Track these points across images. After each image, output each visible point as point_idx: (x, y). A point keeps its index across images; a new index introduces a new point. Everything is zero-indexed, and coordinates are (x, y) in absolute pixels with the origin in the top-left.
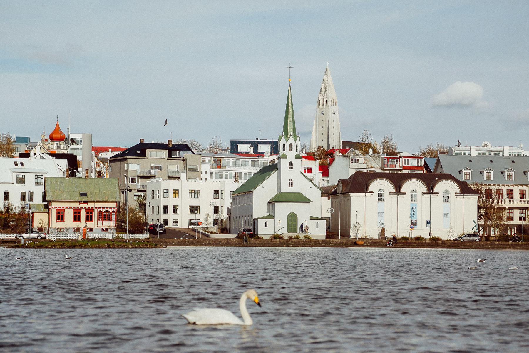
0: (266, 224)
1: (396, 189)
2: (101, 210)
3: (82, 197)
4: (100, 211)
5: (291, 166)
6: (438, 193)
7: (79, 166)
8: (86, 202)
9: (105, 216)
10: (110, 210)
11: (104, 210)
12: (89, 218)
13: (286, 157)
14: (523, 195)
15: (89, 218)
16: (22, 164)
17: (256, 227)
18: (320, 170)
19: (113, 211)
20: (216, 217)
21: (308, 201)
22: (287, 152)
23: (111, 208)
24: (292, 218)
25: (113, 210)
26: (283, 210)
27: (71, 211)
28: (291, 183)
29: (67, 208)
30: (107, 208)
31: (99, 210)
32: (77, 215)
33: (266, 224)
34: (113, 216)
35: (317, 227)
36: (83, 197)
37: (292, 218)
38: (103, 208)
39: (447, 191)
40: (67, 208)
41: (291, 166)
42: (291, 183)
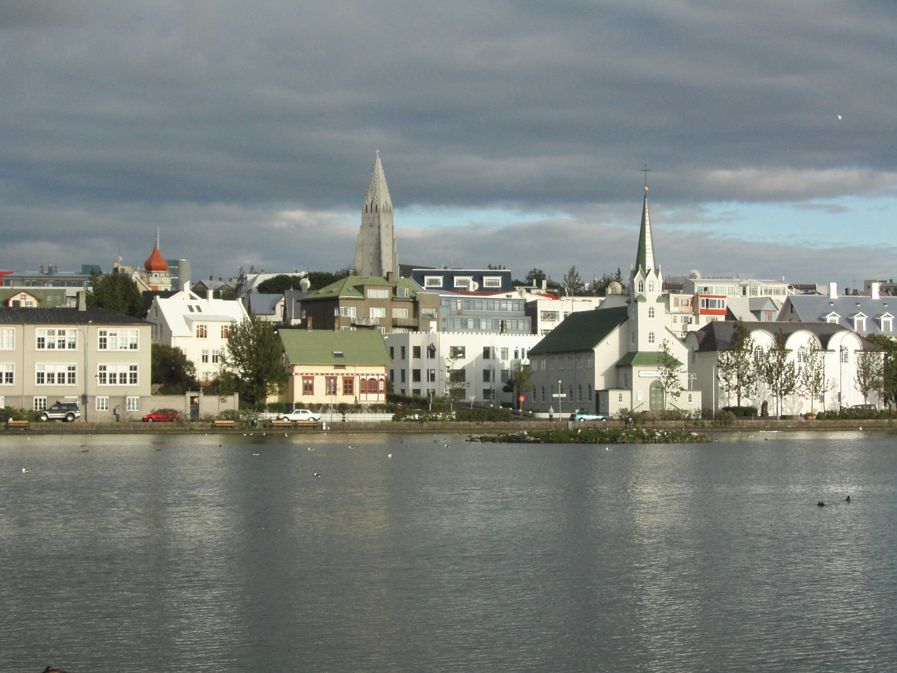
0: (690, 397)
2: (364, 377)
3: (400, 372)
5: (651, 313)
7: (316, 331)
8: (343, 366)
9: (370, 386)
10: (376, 377)
11: (369, 377)
15: (348, 390)
16: (199, 309)
17: (601, 402)
18: (541, 272)
19: (382, 380)
20: (487, 386)
23: (378, 375)
25: (380, 377)
27: (323, 378)
29: (317, 374)
30: (373, 375)
31: (362, 377)
32: (348, 384)
33: (690, 397)
34: (382, 386)
35: (690, 401)
36: (338, 359)
38: (368, 375)
40: (317, 374)
41: (651, 313)
42: (652, 338)
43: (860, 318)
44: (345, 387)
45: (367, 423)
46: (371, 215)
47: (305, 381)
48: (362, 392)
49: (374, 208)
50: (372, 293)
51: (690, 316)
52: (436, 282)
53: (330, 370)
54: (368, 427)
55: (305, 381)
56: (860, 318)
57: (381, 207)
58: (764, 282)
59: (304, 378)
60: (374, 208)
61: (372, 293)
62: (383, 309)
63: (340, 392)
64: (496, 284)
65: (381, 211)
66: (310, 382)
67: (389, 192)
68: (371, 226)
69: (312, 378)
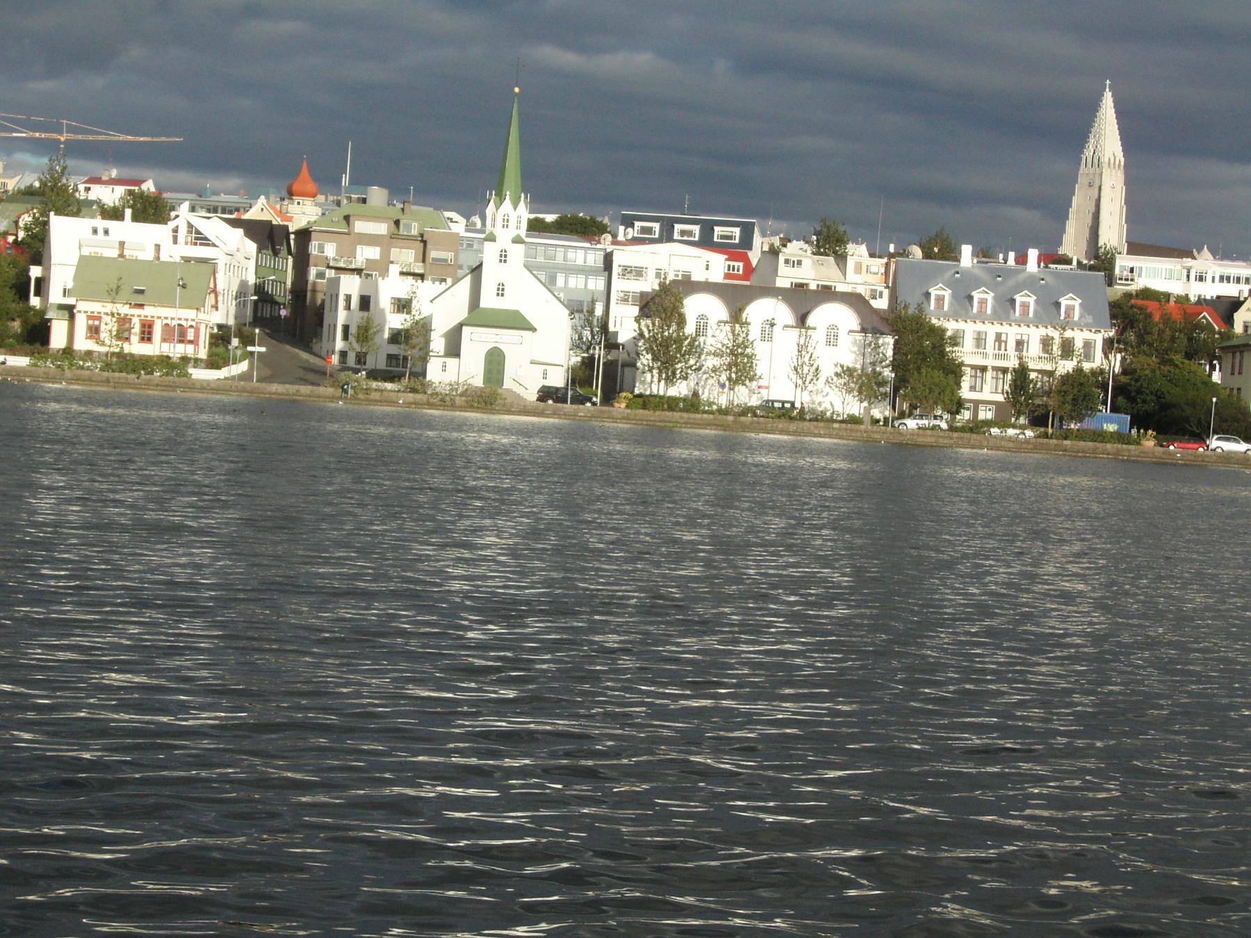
0: (445, 366)
1: (731, 316)
2: (168, 321)
4: (167, 325)
5: (503, 257)
6: (402, 273)
8: (141, 306)
11: (175, 323)
12: (146, 336)
13: (491, 238)
14: (95, 231)
16: (106, 232)
21: (534, 330)
22: (498, 231)
24: (495, 361)
25: (190, 323)
26: (476, 343)
28: (501, 291)
31: (165, 322)
33: (445, 366)
37: (495, 361)
39: (833, 327)
41: (503, 257)
42: (501, 291)
43: (982, 296)
44: (143, 332)
45: (208, 382)
46: (1092, 171)
47: (91, 322)
48: (164, 340)
49: (1096, 161)
50: (360, 226)
51: (880, 289)
52: (690, 233)
53: (125, 310)
54: (212, 385)
55: (91, 322)
56: (982, 296)
57: (1105, 160)
58: (1221, 266)
59: (89, 318)
60: (1096, 161)
61: (360, 226)
62: (378, 249)
63: (135, 339)
64: (730, 238)
65: (1105, 166)
66: (97, 323)
67: (1121, 140)
68: (1090, 185)
69: (99, 318)
